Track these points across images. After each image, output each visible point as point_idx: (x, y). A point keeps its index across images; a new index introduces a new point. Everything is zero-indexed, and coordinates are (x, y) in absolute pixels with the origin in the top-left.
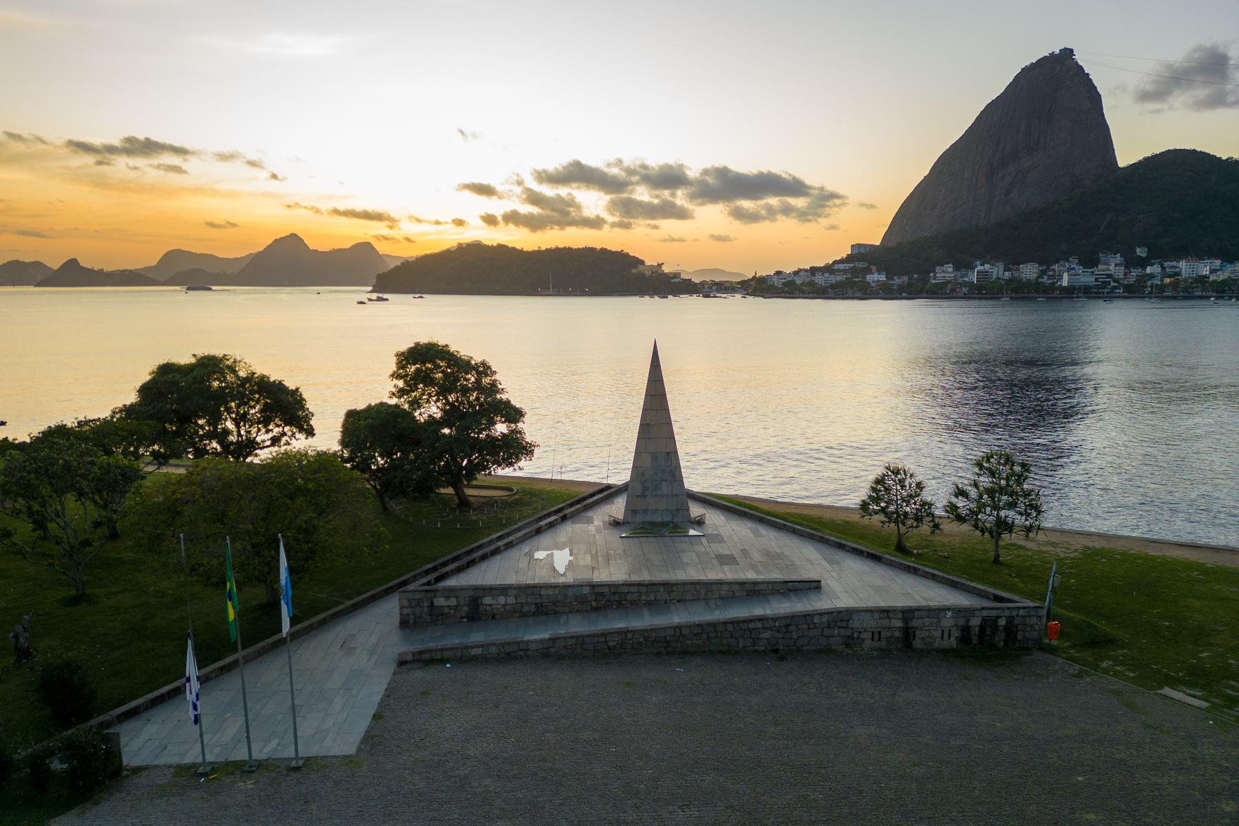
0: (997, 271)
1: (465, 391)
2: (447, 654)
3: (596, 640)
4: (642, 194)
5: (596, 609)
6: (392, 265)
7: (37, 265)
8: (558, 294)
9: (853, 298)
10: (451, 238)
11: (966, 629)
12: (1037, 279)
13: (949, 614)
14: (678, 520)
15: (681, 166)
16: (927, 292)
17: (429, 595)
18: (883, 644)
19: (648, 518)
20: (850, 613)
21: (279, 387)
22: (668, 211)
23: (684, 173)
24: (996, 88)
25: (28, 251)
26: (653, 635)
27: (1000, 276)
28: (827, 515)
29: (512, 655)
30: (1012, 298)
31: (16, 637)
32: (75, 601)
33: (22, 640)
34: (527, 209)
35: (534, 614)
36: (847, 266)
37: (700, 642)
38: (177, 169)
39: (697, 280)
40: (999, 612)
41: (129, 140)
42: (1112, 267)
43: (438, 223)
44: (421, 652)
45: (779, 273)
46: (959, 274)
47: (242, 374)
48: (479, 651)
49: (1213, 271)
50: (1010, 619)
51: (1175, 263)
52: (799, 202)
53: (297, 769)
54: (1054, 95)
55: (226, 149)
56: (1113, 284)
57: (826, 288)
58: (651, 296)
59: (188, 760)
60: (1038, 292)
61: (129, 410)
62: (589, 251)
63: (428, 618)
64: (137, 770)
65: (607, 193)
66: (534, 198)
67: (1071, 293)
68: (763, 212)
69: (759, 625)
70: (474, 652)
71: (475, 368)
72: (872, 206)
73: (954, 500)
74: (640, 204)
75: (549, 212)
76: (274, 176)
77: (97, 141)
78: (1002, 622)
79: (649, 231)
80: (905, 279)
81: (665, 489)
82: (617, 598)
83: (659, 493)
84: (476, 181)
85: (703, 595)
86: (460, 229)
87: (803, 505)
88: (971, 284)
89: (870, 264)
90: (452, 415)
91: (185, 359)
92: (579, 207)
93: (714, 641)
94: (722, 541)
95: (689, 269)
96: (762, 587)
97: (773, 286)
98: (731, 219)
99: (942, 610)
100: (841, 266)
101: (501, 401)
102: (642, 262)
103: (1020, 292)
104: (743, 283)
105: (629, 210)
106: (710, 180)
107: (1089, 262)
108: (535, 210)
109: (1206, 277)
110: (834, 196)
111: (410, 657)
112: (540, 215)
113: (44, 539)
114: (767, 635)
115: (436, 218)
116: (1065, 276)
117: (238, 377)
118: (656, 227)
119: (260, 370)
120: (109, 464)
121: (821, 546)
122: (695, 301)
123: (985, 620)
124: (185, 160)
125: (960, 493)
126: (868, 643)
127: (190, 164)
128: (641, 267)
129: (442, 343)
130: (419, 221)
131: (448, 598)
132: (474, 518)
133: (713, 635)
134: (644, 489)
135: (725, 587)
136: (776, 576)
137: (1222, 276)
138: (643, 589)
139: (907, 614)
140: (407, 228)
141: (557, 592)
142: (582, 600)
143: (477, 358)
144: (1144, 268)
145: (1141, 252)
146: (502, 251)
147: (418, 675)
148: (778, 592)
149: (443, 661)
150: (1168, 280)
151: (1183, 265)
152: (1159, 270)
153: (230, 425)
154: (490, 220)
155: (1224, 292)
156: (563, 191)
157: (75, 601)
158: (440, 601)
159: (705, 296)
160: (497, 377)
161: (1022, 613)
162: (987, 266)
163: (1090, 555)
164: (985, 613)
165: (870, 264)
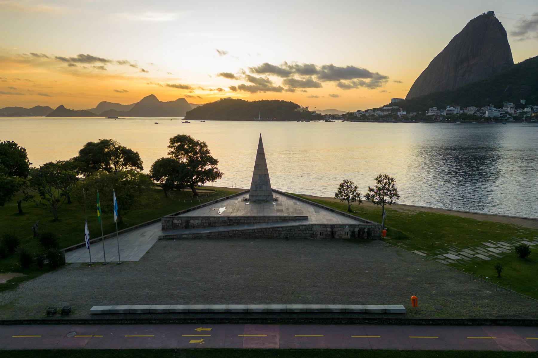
0: (457, 110)
1: (196, 153)
2: (175, 237)
4: (297, 77)
6: (193, 107)
7: (47, 108)
8: (262, 120)
10: (218, 96)
11: (353, 232)
12: (474, 113)
13: (347, 227)
15: (313, 65)
16: (424, 119)
18: (324, 236)
19: (258, 198)
20: (313, 225)
21: (130, 151)
22: (310, 84)
23: (315, 68)
25: (43, 102)
27: (458, 112)
29: (197, 237)
31: (34, 228)
32: (54, 221)
33: (36, 229)
34: (249, 84)
36: (389, 108)
38: (102, 68)
39: (323, 114)
40: (365, 227)
41: (81, 56)
42: (509, 109)
43: (211, 90)
44: (166, 236)
45: (359, 111)
46: (439, 112)
47: (117, 146)
48: (186, 236)
50: (369, 229)
52: (367, 80)
53: (120, 264)
55: (121, 59)
56: (508, 116)
58: (302, 121)
59: (86, 261)
60: (473, 119)
61: (75, 159)
62: (276, 102)
64: (70, 264)
65: (282, 77)
66: (251, 79)
67: (488, 120)
68: (352, 85)
69: (281, 229)
70: (184, 236)
71: (200, 144)
72: (400, 82)
73: (369, 192)
74: (297, 81)
75: (258, 85)
76: (143, 70)
77: (67, 57)
78: (366, 230)
79: (302, 93)
80: (415, 113)
81: (264, 188)
84: (226, 72)
85: (267, 221)
86: (220, 93)
88: (444, 116)
90: (191, 160)
91: (96, 141)
92: (270, 82)
95: (321, 109)
96: (287, 218)
97: (356, 116)
98: (338, 88)
99: (346, 225)
100: (387, 108)
102: (299, 106)
103: (465, 119)
104: (343, 115)
105: (293, 84)
106: (326, 71)
107: (499, 106)
108: (252, 84)
110: (385, 78)
111: (162, 238)
112: (254, 86)
113: (44, 199)
114: (284, 232)
115: (210, 87)
116: (487, 112)
117: (115, 147)
118: (305, 91)
119: (123, 145)
120: (66, 174)
122: (321, 123)
123: (360, 229)
124: (105, 64)
125: (371, 190)
126: (319, 236)
127: (108, 66)
129: (187, 135)
130: (203, 89)
131: (178, 220)
134: (256, 188)
135: (274, 218)
138: (246, 219)
139: (333, 226)
140: (197, 92)
143: (201, 141)
144: (524, 109)
145: (523, 102)
146: (239, 102)
147: (164, 242)
148: (293, 220)
149: (173, 239)
150: (533, 114)
152: (530, 110)
153: (112, 166)
154: (233, 89)
156: (263, 76)
157: (54, 221)
158: (175, 221)
160: (208, 148)
161: (373, 227)
162: (452, 108)
163: (421, 214)
164: (360, 226)
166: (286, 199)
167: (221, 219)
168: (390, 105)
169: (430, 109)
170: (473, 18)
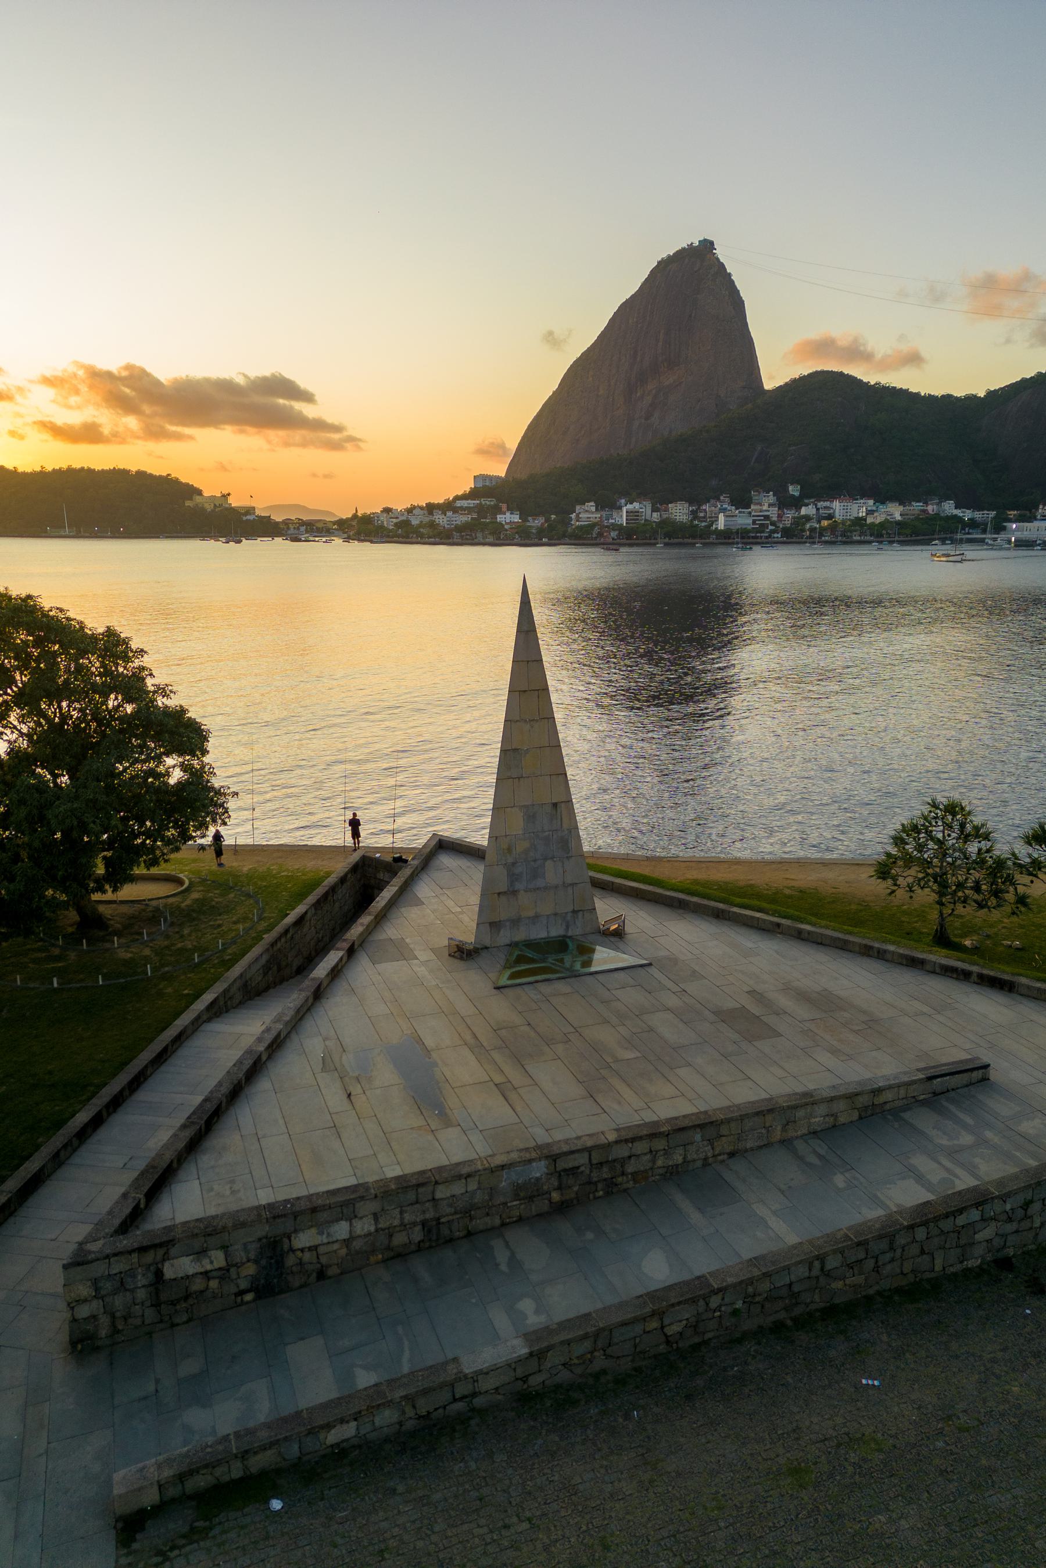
0: (643, 508)
3: (638, 1329)
5: (562, 1208)
8: (78, 536)
9: (484, 544)
14: (575, 931)
16: (570, 537)
17: (149, 1257)
19: (521, 934)
24: (631, 286)
26: (765, 1286)
28: (760, 879)
30: (666, 544)
35: (419, 1248)
36: (471, 503)
37: (860, 1279)
39: (278, 518)
45: (387, 510)
46: (604, 514)
49: (870, 512)
51: (827, 504)
54: (688, 302)
56: (771, 527)
57: (451, 530)
60: (694, 537)
63: (150, 1314)
67: (728, 537)
81: (552, 874)
82: (605, 1173)
83: (540, 883)
88: (619, 528)
89: (500, 500)
97: (382, 527)
101: (166, 711)
102: (199, 492)
103: (676, 535)
107: (742, 502)
109: (864, 519)
114: (987, 1233)
116: (721, 517)
132: (124, 955)
133: (888, 1256)
134: (513, 878)
135: (822, 1110)
137: (878, 518)
138: (660, 1144)
141: (473, 1186)
142: (529, 1192)
143: (96, 625)
144: (798, 509)
145: (794, 490)
149: (253, 1488)
151: (837, 506)
152: (814, 511)
155: (882, 536)
158: (181, 1266)
165: (500, 500)
167: (504, 1183)
168: (473, 494)
169: (578, 507)
170: (664, 256)
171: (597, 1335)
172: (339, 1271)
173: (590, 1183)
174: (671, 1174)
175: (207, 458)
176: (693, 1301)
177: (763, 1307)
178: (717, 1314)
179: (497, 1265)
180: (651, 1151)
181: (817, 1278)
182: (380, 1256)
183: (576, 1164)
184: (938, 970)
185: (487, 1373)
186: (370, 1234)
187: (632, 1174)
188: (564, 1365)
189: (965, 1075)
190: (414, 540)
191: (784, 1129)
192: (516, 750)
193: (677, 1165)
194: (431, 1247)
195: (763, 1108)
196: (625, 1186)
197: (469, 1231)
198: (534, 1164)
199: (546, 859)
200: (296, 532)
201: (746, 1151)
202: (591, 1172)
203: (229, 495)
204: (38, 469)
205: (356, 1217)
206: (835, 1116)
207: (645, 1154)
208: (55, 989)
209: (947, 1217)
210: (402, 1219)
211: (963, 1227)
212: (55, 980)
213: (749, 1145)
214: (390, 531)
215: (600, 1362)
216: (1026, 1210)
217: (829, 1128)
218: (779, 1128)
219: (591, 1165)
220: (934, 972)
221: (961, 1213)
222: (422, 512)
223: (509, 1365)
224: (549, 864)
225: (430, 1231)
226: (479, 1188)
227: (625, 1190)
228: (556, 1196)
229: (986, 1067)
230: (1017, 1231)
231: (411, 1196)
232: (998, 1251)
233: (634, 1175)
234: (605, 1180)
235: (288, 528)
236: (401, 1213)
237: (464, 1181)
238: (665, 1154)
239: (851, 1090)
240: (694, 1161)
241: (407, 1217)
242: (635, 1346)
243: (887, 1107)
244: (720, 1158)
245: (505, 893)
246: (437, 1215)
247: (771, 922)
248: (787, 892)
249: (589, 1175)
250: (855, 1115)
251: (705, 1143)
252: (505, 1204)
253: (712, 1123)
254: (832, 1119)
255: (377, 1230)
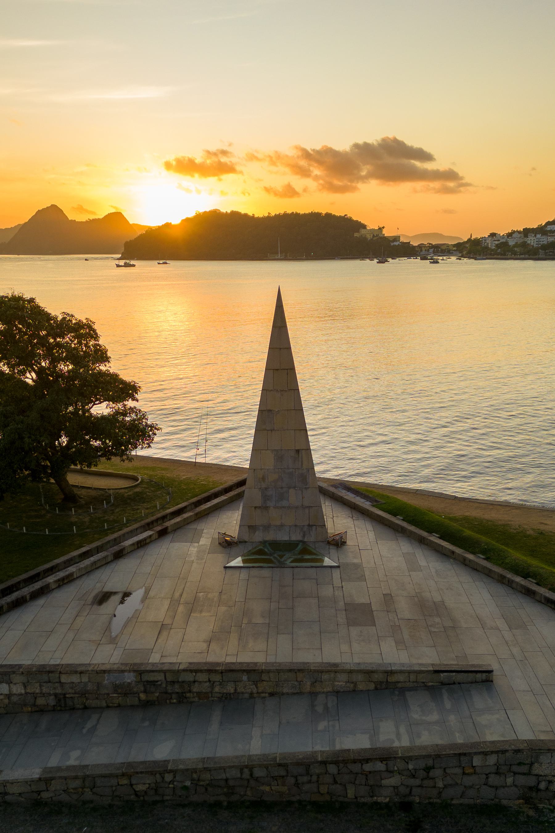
3: (114, 782)
5: (146, 705)
8: (286, 259)
14: (310, 538)
19: (271, 536)
26: (207, 776)
35: (54, 709)
37: (285, 789)
39: (415, 243)
45: (493, 235)
57: (538, 248)
81: (293, 498)
83: (285, 503)
85: (307, 687)
87: (486, 500)
93: (306, 787)
94: (362, 578)
97: (487, 248)
102: (364, 227)
121: (501, 590)
122: (415, 263)
128: (363, 231)
134: (266, 498)
136: (426, 656)
138: (216, 678)
141: (85, 679)
142: (125, 691)
143: (80, 316)
159: (422, 259)
166: (372, 535)
167: (107, 680)
171: (85, 778)
172: (5, 712)
173: (166, 693)
174: (226, 698)
175: (372, 203)
176: (153, 773)
177: (206, 789)
178: (171, 786)
179: (83, 728)
180: (209, 681)
181: (248, 780)
182: (30, 709)
183: (156, 679)
184: (543, 601)
185: (12, 783)
186: (21, 694)
187: (196, 693)
188: (64, 791)
189: (470, 674)
190: (509, 257)
191: (313, 684)
192: (270, 411)
193: (230, 694)
194: (61, 710)
195: (296, 668)
196: (192, 700)
197: (85, 706)
198: (126, 674)
199: (289, 488)
200: (427, 253)
201: (283, 694)
202: (167, 686)
203: (383, 228)
204: (266, 215)
205: (12, 683)
206: (355, 684)
207: (206, 682)
208: (47, 535)
209: (355, 763)
210: (41, 690)
211: (370, 772)
212: (24, 528)
213: (285, 690)
214: (492, 250)
215: (88, 795)
216: (428, 773)
217: (349, 691)
218: (309, 683)
219: (167, 682)
220: (540, 602)
221: (367, 762)
222: (519, 235)
223: (27, 782)
224: (291, 491)
225: (60, 700)
226: (89, 681)
227: (192, 703)
228: (143, 696)
229: (491, 671)
230: (421, 786)
231: (45, 677)
232: (405, 796)
233: (199, 694)
234: (177, 693)
235: (421, 251)
236: (41, 686)
237: (79, 675)
238: (220, 685)
239: (369, 668)
240: (243, 693)
241: (45, 690)
242: (113, 792)
243: (400, 685)
244: (263, 695)
245: (260, 507)
246: (64, 692)
247: (450, 550)
248: (530, 532)
249: (166, 688)
250: (372, 686)
251: (250, 683)
252: (108, 694)
253: (254, 670)
254: (352, 685)
255: (26, 693)
